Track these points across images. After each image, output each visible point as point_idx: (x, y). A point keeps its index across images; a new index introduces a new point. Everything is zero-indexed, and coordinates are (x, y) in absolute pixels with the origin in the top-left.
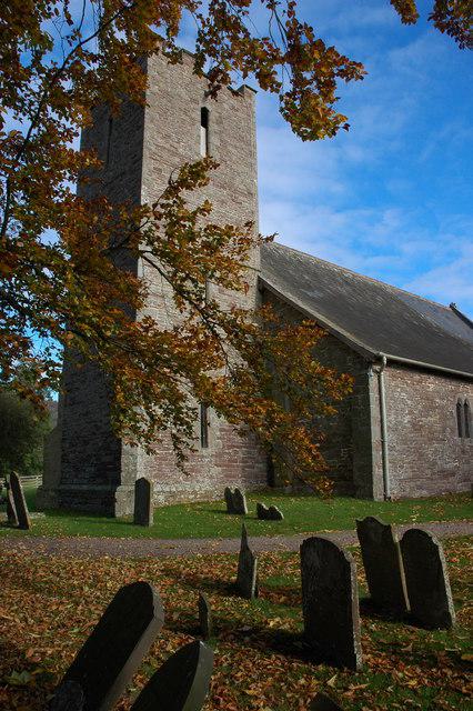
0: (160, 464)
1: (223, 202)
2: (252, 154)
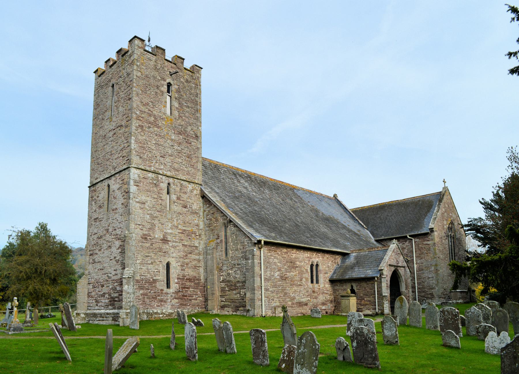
0: (144, 298)
1: (180, 143)
2: (198, 111)
